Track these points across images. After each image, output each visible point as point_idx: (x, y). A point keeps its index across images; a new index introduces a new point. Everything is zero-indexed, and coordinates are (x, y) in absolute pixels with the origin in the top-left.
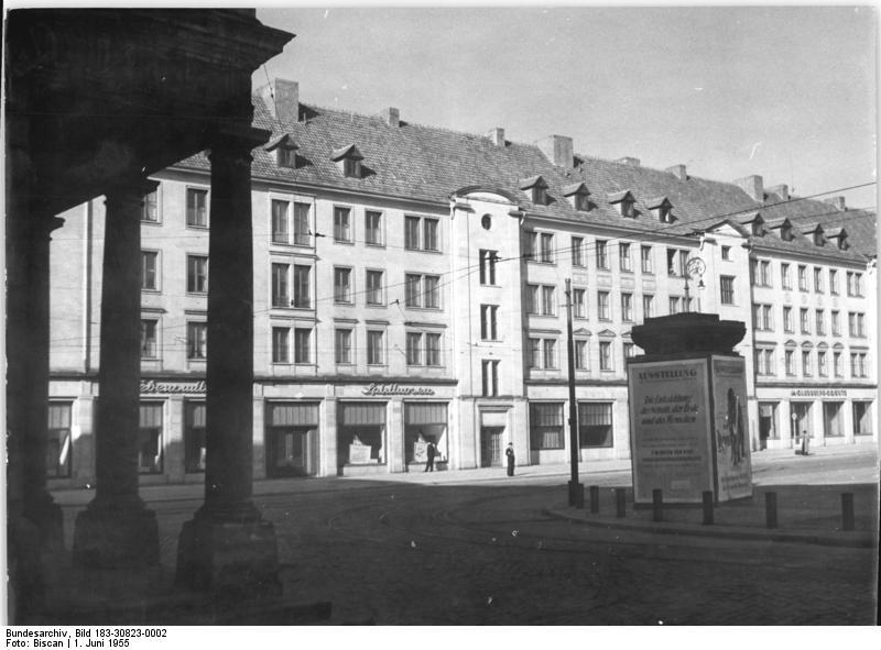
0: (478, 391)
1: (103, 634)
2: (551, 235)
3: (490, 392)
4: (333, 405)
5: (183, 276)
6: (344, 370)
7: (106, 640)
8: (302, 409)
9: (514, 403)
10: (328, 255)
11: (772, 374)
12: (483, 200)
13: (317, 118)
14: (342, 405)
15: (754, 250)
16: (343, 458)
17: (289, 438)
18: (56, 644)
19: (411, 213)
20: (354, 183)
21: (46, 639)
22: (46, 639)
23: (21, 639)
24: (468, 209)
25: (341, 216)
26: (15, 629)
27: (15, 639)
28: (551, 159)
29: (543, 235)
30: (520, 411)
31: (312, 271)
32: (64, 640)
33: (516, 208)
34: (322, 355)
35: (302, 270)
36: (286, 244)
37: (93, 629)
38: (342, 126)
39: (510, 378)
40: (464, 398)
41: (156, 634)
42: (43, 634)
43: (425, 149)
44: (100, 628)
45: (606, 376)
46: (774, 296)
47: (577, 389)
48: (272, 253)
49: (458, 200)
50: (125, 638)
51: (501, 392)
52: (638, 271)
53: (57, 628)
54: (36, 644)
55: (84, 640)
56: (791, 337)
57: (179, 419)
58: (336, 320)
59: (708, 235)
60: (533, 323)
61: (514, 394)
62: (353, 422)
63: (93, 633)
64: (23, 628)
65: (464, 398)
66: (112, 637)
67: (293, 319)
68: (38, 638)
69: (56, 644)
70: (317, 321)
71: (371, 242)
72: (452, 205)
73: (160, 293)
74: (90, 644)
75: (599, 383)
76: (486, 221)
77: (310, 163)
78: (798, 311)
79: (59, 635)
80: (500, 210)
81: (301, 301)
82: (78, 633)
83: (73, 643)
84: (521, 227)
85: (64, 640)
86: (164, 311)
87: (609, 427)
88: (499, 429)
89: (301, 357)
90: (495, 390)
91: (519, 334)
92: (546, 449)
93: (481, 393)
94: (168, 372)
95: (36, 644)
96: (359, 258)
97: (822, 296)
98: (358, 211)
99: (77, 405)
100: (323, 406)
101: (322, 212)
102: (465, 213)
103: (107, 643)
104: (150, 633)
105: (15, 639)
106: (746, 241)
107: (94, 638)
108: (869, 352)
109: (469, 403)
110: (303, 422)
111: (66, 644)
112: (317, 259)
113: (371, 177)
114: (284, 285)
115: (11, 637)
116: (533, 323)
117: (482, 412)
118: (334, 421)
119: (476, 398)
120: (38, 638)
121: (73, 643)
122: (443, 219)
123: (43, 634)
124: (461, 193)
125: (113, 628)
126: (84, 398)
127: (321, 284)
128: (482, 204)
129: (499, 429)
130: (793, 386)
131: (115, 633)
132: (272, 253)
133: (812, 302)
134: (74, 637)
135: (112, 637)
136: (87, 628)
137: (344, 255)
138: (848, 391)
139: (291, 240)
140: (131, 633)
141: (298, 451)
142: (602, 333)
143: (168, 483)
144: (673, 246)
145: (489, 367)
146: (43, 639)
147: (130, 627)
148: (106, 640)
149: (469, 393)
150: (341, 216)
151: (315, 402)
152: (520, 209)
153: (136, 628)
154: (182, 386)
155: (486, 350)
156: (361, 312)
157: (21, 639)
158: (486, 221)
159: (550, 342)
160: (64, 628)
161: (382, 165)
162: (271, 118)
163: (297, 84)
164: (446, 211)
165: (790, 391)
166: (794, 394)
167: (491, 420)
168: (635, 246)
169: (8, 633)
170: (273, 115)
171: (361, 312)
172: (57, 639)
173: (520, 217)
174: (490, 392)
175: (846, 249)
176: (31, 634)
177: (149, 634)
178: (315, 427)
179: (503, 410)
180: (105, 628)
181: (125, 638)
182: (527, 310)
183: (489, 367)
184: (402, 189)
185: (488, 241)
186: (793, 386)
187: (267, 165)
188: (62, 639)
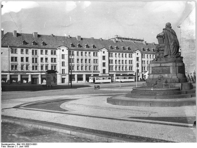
0: (61, 73)
1: (23, 144)
2: (74, 52)
3: (63, 73)
4: (40, 75)
5: (50, 53)
6: (42, 71)
7: (24, 146)
8: (36, 76)
9: (67, 75)
10: (40, 56)
11: (117, 70)
12: (62, 47)
13: (41, 37)
14: (42, 75)
15: (109, 52)
16: (42, 82)
17: (35, 79)
18: (13, 147)
19: (52, 50)
20: (44, 47)
21: (10, 145)
22: (10, 145)
23: (5, 145)
24: (60, 49)
25: (42, 51)
26: (3, 143)
27: (3, 146)
28: (77, 39)
29: (72, 52)
30: (67, 76)
31: (38, 58)
32: (14, 146)
33: (68, 48)
34: (19, 69)
35: (36, 59)
36: (34, 55)
37: (21, 143)
38: (44, 38)
39: (66, 71)
40: (59, 74)
41: (35, 144)
42: (10, 145)
43: (56, 40)
44: (22, 143)
45: (82, 71)
46: (114, 59)
47: (72, 73)
48: (32, 56)
49: (59, 48)
50: (28, 145)
51: (65, 73)
52: (88, 56)
53: (13, 143)
54: (8, 147)
55: (19, 146)
56: (120, 64)
57: (20, 77)
58: (41, 64)
59: (100, 50)
60: (143, 65)
61: (67, 73)
62: (44, 77)
63: (21, 144)
64: (5, 143)
65: (59, 74)
66: (25, 145)
67: (35, 64)
68: (9, 145)
69: (13, 147)
70: (38, 65)
71: (46, 54)
72: (58, 48)
73: (24, 62)
74: (20, 147)
75: (81, 72)
76: (63, 50)
77: (38, 44)
78: (122, 61)
79: (13, 145)
80: (65, 49)
81: (36, 62)
82: (17, 144)
83: (16, 146)
84: (68, 51)
85: (14, 146)
86: (18, 64)
87: (83, 78)
88: (65, 78)
89: (36, 69)
90: (64, 73)
91: (108, 66)
92: (73, 81)
93: (62, 73)
94: (19, 71)
95: (8, 147)
96: (44, 56)
97: (117, 58)
98: (44, 50)
99: (8, 75)
100: (39, 75)
101: (39, 51)
102: (59, 50)
104: (34, 144)
105: (3, 146)
106: (108, 50)
107: (21, 145)
108: (133, 66)
109: (60, 75)
110: (36, 77)
111: (15, 147)
112: (38, 57)
113: (46, 45)
114: (34, 60)
116: (110, 64)
117: (62, 76)
118: (40, 77)
119: (61, 74)
120: (9, 145)
121: (16, 146)
122: (57, 50)
123: (10, 145)
124: (59, 47)
125: (25, 143)
126: (9, 75)
127: (39, 60)
128: (62, 48)
129: (65, 78)
130: (116, 72)
131: (26, 144)
132: (32, 56)
133: (121, 59)
134: (16, 145)
135: (25, 145)
136: (19, 143)
137: (42, 56)
138: (128, 73)
139: (35, 54)
140: (29, 144)
141: (36, 81)
142: (119, 65)
143: (19, 84)
144: (94, 52)
145: (63, 70)
146: (10, 146)
147: (29, 143)
148: (24, 146)
149: (60, 73)
150: (42, 51)
151: (38, 75)
152: (68, 48)
153: (30, 143)
154: (20, 73)
155: (63, 68)
156: (125, 65)
157: (5, 145)
158: (63, 50)
159: (112, 67)
160: (14, 143)
161: (49, 43)
162: (34, 38)
163: (37, 33)
164: (57, 49)
165: (116, 73)
166: (116, 73)
167: (63, 77)
168: (88, 52)
169: (2, 144)
170: (34, 37)
171: (88, 64)
172: (13, 146)
173: (68, 49)
174: (63, 73)
175: (130, 50)
176: (7, 144)
177: (33, 144)
178: (38, 78)
179: (65, 76)
180: (24, 143)
181: (28, 145)
182: (109, 63)
183: (63, 70)
184: (51, 47)
185: (63, 53)
186: (116, 72)
187: (31, 45)
188: (14, 145)
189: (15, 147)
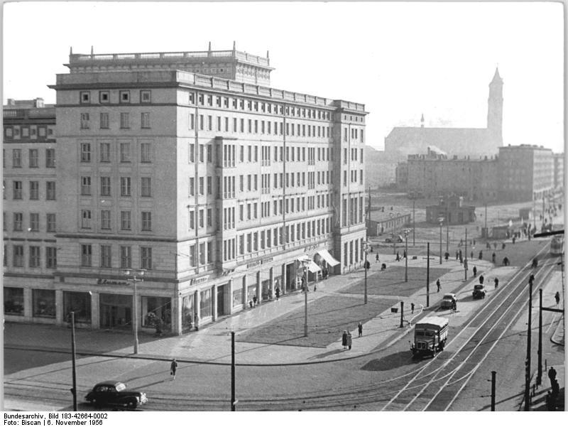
18: (36, 423)
21: (30, 420)
22: (30, 420)
23: (14, 420)
27: (10, 420)
42: (28, 417)
50: (100, 419)
54: (23, 423)
55: (53, 421)
66: (92, 419)
68: (25, 419)
69: (36, 423)
79: (38, 417)
95: (23, 423)
103: (88, 423)
105: (10, 420)
111: (42, 423)
115: (7, 419)
120: (25, 419)
123: (28, 417)
134: (48, 419)
146: (28, 420)
157: (14, 420)
160: (41, 413)
172: (37, 420)
176: (20, 416)
188: (40, 420)
189: (42, 423)
